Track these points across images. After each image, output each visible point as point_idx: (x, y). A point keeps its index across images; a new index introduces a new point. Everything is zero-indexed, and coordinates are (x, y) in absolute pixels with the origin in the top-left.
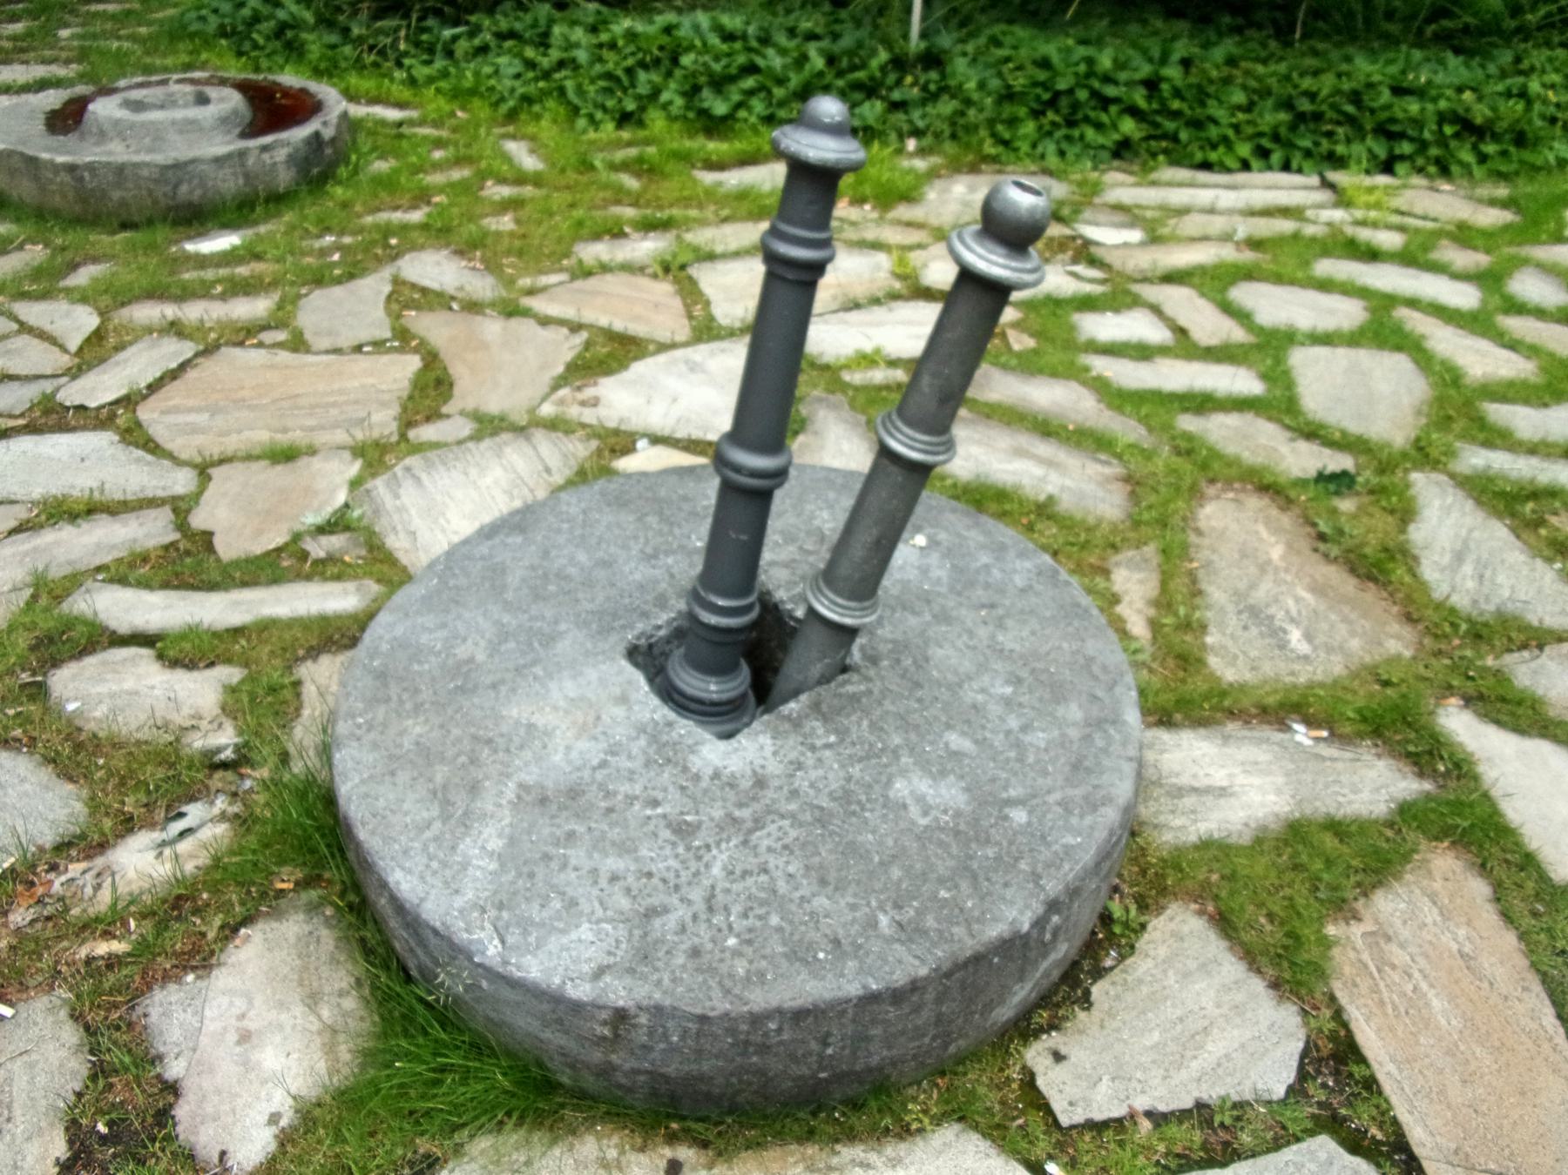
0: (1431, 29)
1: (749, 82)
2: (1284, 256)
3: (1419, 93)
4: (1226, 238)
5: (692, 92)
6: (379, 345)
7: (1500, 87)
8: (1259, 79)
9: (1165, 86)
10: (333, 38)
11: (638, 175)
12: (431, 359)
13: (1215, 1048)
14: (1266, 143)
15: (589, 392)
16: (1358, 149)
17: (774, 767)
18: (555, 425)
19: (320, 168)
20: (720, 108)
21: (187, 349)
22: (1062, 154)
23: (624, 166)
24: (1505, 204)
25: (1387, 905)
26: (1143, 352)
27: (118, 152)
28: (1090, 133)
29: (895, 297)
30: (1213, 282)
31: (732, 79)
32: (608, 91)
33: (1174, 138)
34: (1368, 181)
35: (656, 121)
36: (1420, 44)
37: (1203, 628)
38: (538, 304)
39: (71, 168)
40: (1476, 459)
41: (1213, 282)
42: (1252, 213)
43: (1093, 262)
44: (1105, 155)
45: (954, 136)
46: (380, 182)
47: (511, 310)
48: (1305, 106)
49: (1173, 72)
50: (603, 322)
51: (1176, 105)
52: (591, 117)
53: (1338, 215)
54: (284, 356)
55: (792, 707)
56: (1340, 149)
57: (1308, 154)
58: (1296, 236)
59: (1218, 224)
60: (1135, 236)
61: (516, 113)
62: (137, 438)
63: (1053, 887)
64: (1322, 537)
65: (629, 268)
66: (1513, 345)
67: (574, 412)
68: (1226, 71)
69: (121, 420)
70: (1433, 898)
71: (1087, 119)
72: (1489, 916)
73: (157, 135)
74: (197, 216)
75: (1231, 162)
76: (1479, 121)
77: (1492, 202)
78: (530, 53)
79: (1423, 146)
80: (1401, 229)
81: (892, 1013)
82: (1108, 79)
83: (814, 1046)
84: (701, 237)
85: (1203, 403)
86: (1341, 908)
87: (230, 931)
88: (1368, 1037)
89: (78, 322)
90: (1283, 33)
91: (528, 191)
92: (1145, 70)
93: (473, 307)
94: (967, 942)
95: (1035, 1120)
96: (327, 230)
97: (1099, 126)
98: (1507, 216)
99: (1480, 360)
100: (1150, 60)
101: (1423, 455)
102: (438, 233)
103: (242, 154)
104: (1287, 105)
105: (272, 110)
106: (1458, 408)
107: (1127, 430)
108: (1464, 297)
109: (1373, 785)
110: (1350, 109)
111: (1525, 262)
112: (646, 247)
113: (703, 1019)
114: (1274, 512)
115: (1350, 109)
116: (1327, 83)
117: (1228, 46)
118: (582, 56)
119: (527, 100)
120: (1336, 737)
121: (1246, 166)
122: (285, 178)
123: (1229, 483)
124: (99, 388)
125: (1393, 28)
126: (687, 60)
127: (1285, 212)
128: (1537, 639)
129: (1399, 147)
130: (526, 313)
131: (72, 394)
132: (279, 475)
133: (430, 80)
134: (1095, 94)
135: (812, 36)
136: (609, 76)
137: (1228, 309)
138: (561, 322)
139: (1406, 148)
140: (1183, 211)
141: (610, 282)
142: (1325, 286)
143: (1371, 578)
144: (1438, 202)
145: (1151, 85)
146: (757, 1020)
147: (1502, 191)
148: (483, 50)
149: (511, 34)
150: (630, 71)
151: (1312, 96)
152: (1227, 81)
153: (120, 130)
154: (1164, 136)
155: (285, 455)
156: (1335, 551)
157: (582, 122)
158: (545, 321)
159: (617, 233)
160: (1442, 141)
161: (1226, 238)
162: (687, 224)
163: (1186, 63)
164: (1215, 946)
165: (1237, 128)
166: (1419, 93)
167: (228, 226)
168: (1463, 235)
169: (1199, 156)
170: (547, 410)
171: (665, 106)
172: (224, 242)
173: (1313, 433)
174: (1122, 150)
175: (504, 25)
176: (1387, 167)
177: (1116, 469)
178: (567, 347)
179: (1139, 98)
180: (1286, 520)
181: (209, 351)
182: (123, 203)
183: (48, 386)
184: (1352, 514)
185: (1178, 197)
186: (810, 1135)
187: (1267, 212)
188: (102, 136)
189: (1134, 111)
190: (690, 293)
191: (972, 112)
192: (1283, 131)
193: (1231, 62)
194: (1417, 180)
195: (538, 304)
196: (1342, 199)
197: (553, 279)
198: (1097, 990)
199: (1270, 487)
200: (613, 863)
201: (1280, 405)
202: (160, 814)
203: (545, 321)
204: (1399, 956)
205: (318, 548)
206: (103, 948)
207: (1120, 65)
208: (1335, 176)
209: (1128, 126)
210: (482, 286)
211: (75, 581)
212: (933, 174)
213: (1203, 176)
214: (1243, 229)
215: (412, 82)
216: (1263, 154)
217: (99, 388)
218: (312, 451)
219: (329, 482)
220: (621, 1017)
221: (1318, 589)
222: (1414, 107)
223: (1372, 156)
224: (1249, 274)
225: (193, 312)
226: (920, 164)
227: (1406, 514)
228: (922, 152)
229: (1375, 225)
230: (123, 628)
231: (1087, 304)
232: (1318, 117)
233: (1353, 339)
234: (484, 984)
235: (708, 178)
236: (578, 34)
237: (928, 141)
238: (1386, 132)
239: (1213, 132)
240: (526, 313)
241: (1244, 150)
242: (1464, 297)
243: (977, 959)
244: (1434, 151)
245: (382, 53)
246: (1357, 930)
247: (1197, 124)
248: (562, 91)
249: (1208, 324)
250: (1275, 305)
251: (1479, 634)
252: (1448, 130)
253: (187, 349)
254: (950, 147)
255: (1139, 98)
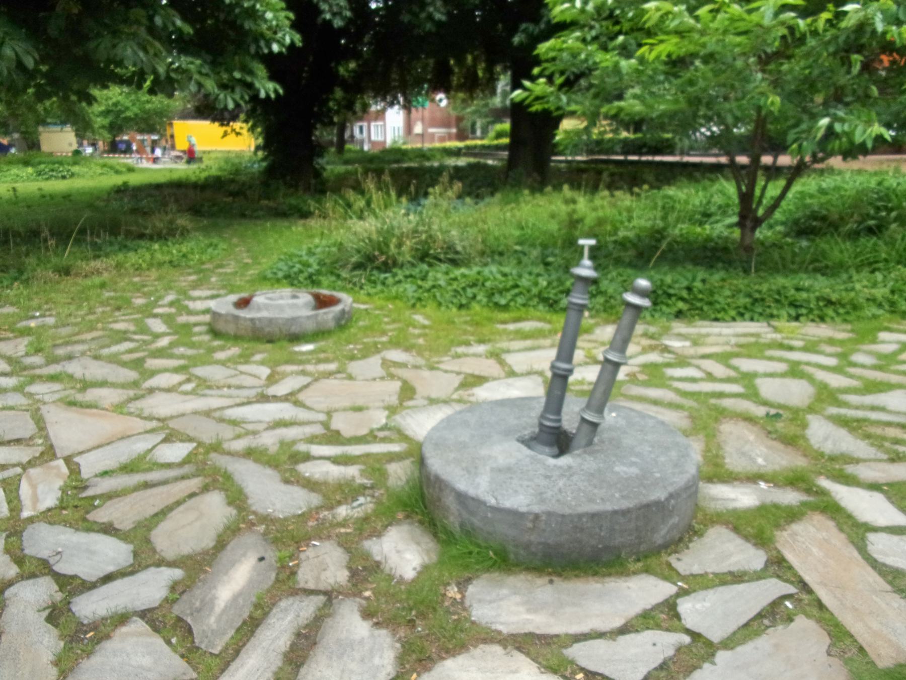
0: (811, 267)
1: (516, 291)
2: (755, 349)
3: (807, 290)
4: (727, 343)
5: (490, 295)
6: (382, 378)
7: (842, 287)
8: (736, 286)
9: (695, 290)
10: (333, 278)
11: (471, 325)
12: (405, 382)
13: (733, 559)
14: (742, 310)
15: (470, 392)
16: (784, 313)
17: (573, 464)
18: (459, 401)
19: (344, 322)
20: (503, 302)
21: (308, 379)
22: (653, 316)
23: (466, 323)
24: (849, 332)
25: (796, 527)
26: (693, 380)
27: (264, 314)
28: (664, 308)
29: (587, 364)
30: (723, 358)
31: (507, 290)
32: (455, 296)
33: (701, 309)
34: (787, 324)
35: (476, 307)
36: (806, 271)
37: (724, 458)
38: (442, 366)
39: (252, 320)
40: (833, 410)
41: (723, 358)
42: (737, 335)
43: (669, 352)
44: (672, 317)
45: (605, 311)
46: (366, 328)
47: (432, 368)
48: (757, 296)
49: (698, 284)
50: (470, 371)
51: (700, 296)
52: (447, 307)
53: (774, 336)
54: (346, 382)
55: (577, 452)
56: (775, 312)
57: (761, 314)
58: (756, 343)
59: (721, 340)
60: (687, 344)
61: (417, 303)
62: (298, 404)
63: (671, 489)
64: (770, 432)
65: (475, 355)
66: (851, 376)
67: (466, 398)
68: (721, 284)
69: (291, 398)
70: (814, 526)
71: (662, 303)
72: (834, 530)
73: (281, 308)
74: (296, 338)
75: (727, 318)
76: (834, 299)
77: (844, 331)
78: (420, 283)
79: (811, 311)
80: (803, 340)
81: (622, 520)
82: (670, 287)
83: (597, 530)
84: (504, 345)
85: (721, 395)
86: (778, 526)
87: (385, 527)
88: (790, 556)
89: (265, 371)
90: (746, 271)
91: (427, 331)
92: (685, 283)
93: (416, 367)
94: (645, 500)
95: (673, 574)
96: (350, 343)
97: (668, 305)
98: (851, 335)
99: (835, 381)
100: (687, 279)
101: (811, 409)
102: (395, 344)
103: (317, 315)
104: (749, 295)
105: (322, 302)
106: (826, 396)
107: (688, 403)
108: (832, 362)
109: (790, 497)
110: (777, 297)
111: (858, 350)
112: (481, 349)
113: (563, 516)
114: (750, 426)
115: (777, 297)
116: (765, 287)
117: (721, 274)
118: (442, 283)
119: (419, 299)
120: (776, 485)
121: (734, 319)
122: (331, 324)
123: (731, 418)
124: (282, 389)
125: (795, 267)
126: (488, 284)
127: (752, 335)
128: (858, 461)
129: (798, 310)
130: (438, 369)
131: (272, 391)
132: (358, 415)
133: (376, 294)
134: (665, 293)
135: (538, 275)
136: (455, 291)
137: (729, 366)
138: (452, 372)
139: (804, 311)
140: (708, 335)
141: (468, 360)
142: (771, 359)
143: (789, 444)
144: (822, 331)
145: (689, 289)
146: (580, 516)
147: (849, 327)
148: (400, 282)
149: (411, 276)
150: (464, 289)
151: (760, 292)
152: (722, 287)
153: (267, 307)
154: (697, 309)
155: (359, 409)
156: (774, 436)
157: (443, 309)
158: (446, 371)
159: (468, 344)
160: (820, 309)
161: (727, 343)
162: (495, 341)
163: (704, 281)
164: (732, 535)
165: (728, 305)
166: (807, 290)
167: (308, 342)
168: (831, 341)
169: (713, 316)
170: (455, 396)
171: (479, 302)
172: (309, 347)
173: (765, 403)
174: (679, 314)
175: (407, 273)
176: (797, 318)
177: (686, 413)
178: (457, 380)
179: (684, 294)
180: (755, 429)
181: (316, 380)
182: (269, 333)
183: (259, 390)
184: (782, 425)
185: (704, 331)
186: (595, 574)
187: (745, 335)
188: (259, 309)
189: (682, 299)
190: (502, 363)
191: (612, 301)
192: (749, 306)
193: (723, 280)
194: (810, 324)
195: (442, 366)
196: (776, 330)
197: (446, 359)
198: (691, 545)
199: (749, 419)
200: (526, 483)
201: (753, 394)
202: (350, 500)
203: (446, 371)
204: (799, 538)
205: (381, 434)
206: (343, 530)
207: (675, 282)
208: (775, 323)
209: (681, 305)
210: (420, 361)
211: (294, 442)
212: (597, 325)
213: (715, 324)
214: (733, 340)
215: (369, 295)
216: (742, 315)
217: (282, 389)
218: (367, 408)
219: (380, 418)
220: (537, 517)
221: (767, 447)
222: (804, 295)
223: (789, 315)
224: (737, 355)
225: (310, 368)
226: (592, 321)
227: (805, 426)
228: (591, 317)
229: (792, 339)
230: (208, 542)
231: (669, 365)
232: (763, 300)
233: (783, 375)
234: (489, 515)
235: (501, 327)
236: (439, 275)
237: (593, 312)
238: (793, 304)
239: (718, 306)
240: (438, 369)
241: (733, 313)
242: (832, 362)
243: (648, 506)
244: (816, 312)
245: (355, 284)
246: (785, 533)
247: (710, 304)
248: (435, 296)
249: (719, 370)
250: (746, 365)
251: (832, 459)
252: (821, 304)
253: (308, 379)
254: (604, 315)
255: (684, 294)
